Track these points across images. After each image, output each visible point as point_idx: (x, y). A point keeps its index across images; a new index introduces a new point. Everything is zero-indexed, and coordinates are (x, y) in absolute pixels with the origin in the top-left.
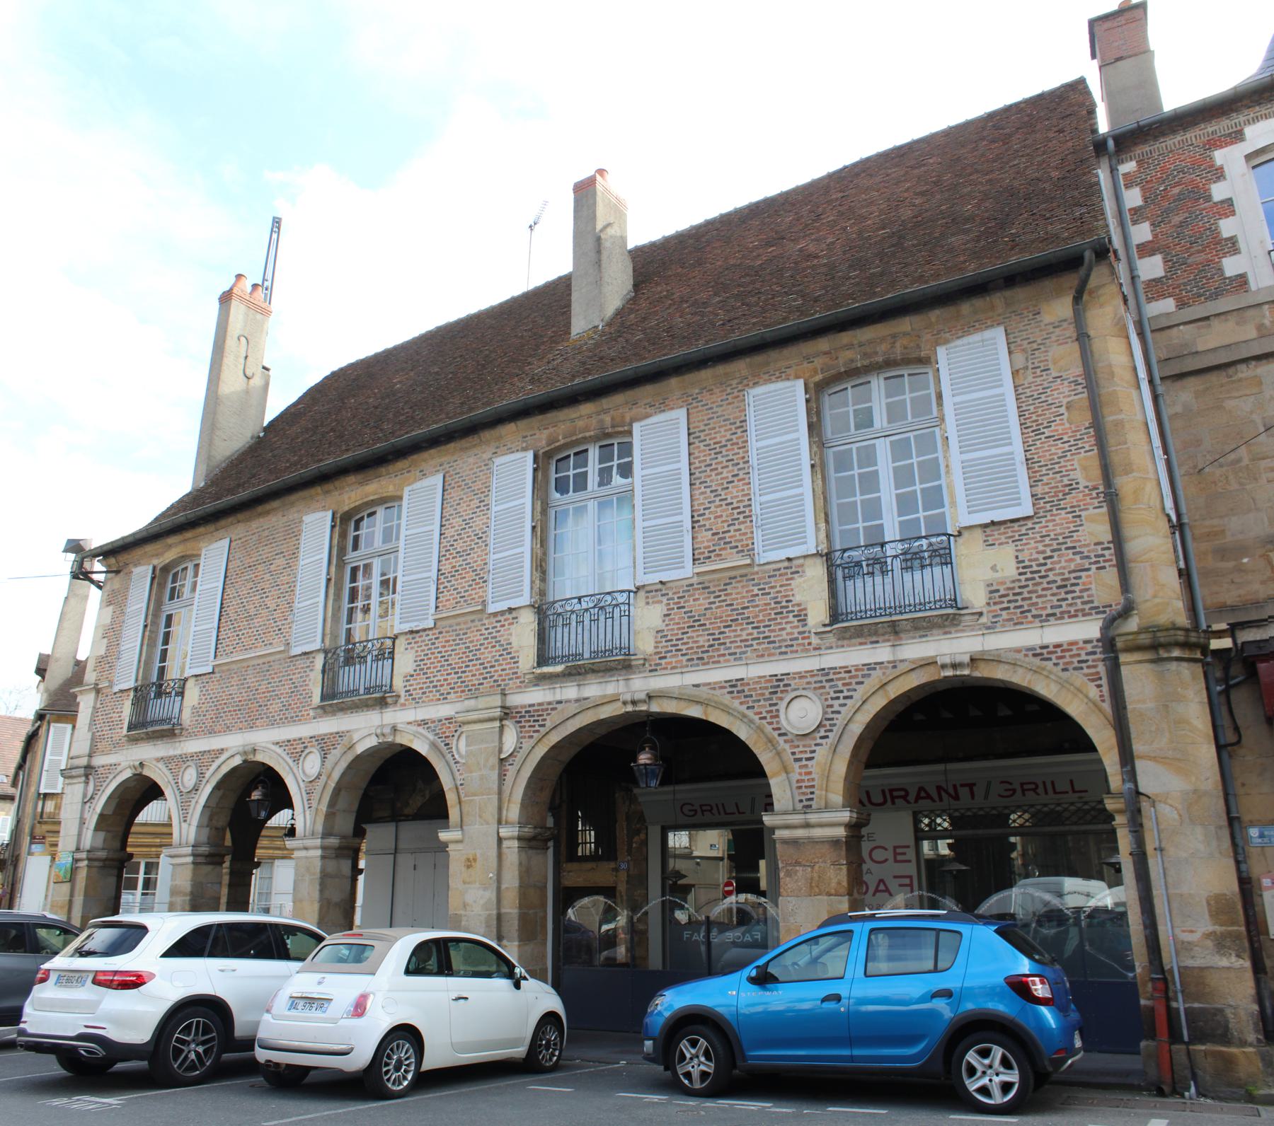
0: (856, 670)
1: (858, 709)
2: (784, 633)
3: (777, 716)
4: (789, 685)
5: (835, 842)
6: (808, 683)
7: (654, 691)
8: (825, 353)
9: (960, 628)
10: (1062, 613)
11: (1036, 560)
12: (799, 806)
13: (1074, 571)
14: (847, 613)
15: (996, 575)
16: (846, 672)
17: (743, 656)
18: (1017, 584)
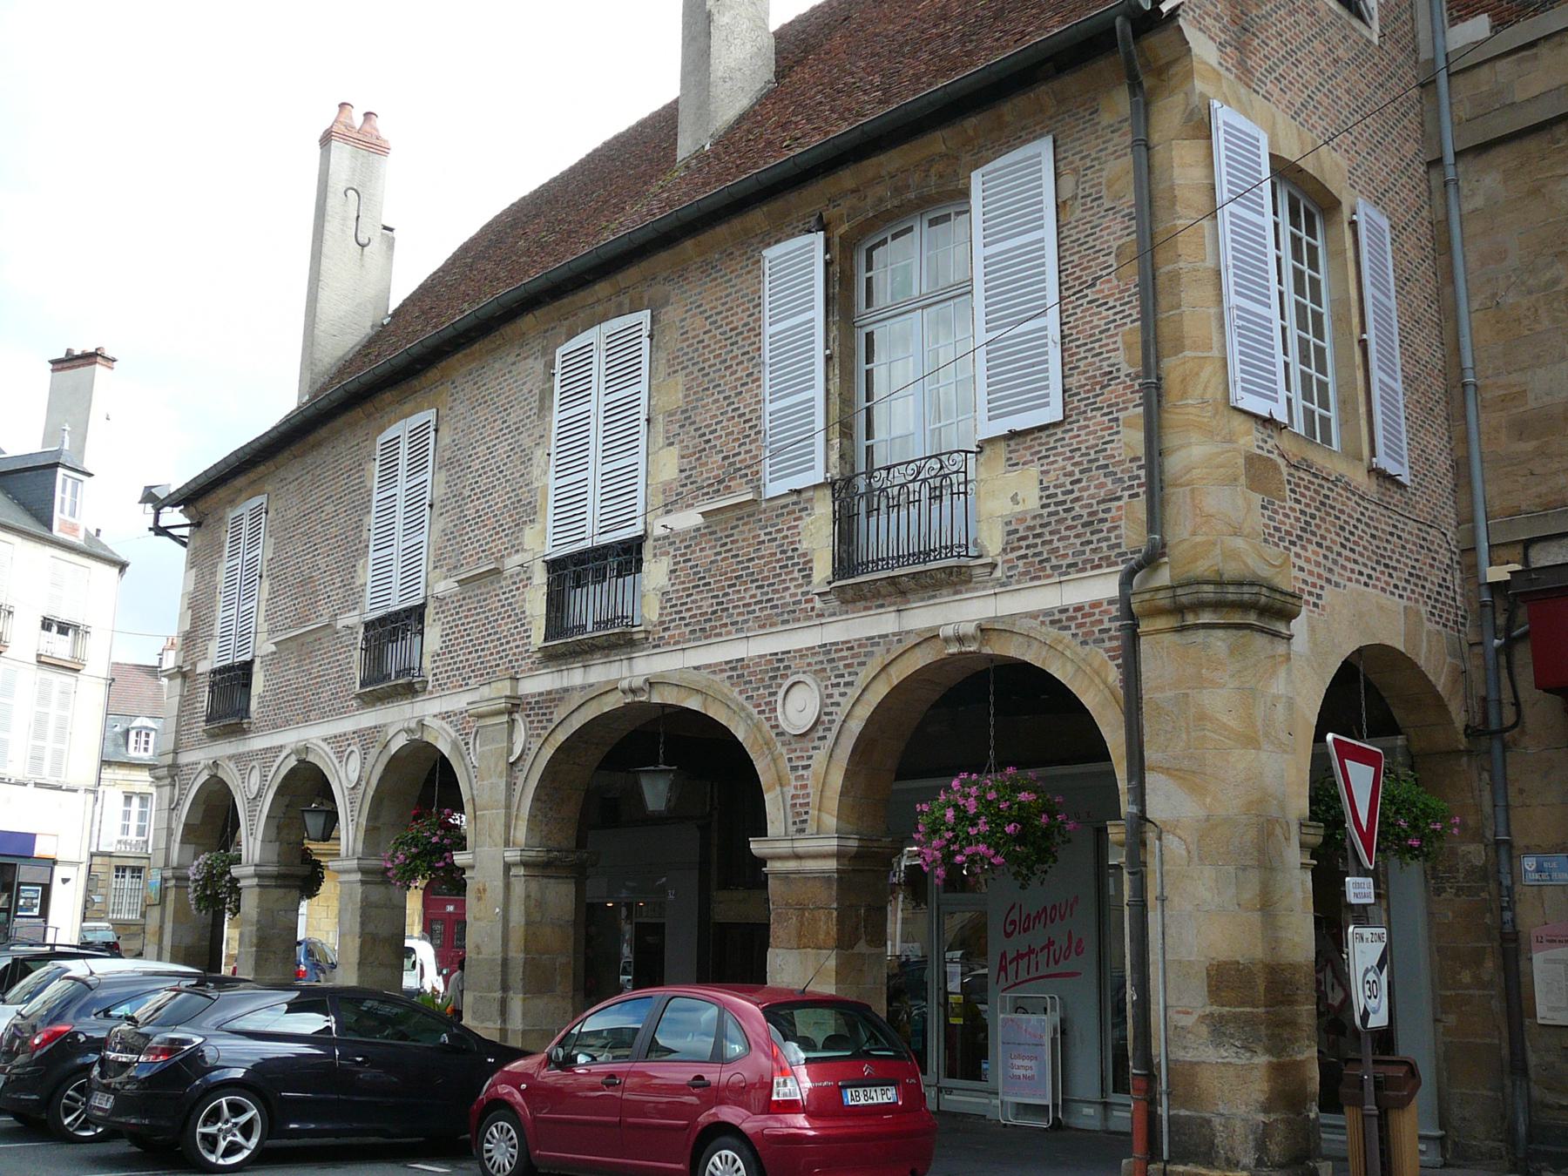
0: (860, 646)
1: (858, 699)
2: (787, 594)
3: (775, 710)
4: (789, 667)
5: (823, 878)
6: (809, 664)
7: (655, 675)
8: (853, 192)
9: (972, 585)
10: (1085, 562)
11: (1063, 485)
12: (792, 829)
13: (1104, 501)
14: (899, 556)
15: (1018, 508)
16: (848, 649)
17: (745, 626)
18: (1038, 521)
